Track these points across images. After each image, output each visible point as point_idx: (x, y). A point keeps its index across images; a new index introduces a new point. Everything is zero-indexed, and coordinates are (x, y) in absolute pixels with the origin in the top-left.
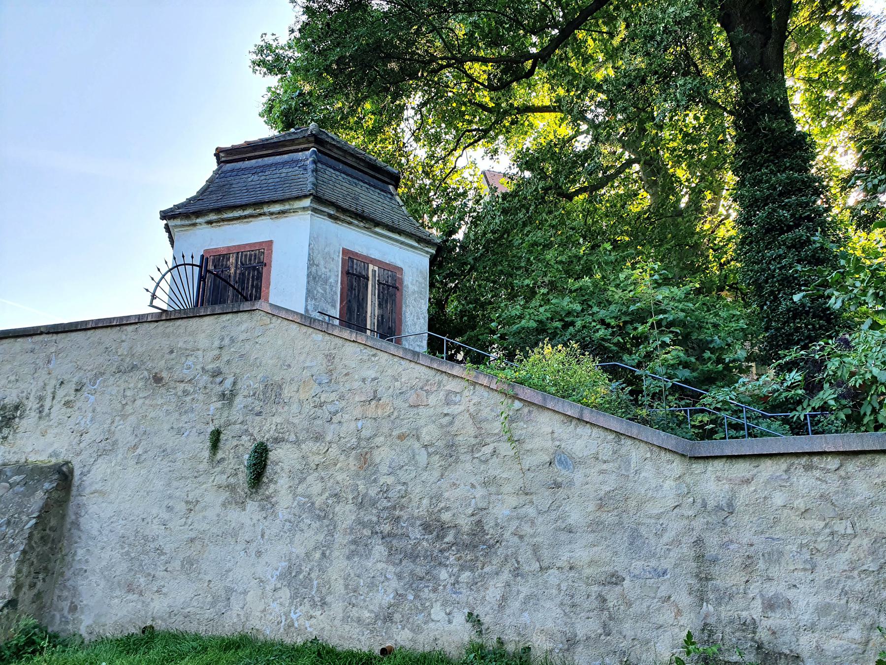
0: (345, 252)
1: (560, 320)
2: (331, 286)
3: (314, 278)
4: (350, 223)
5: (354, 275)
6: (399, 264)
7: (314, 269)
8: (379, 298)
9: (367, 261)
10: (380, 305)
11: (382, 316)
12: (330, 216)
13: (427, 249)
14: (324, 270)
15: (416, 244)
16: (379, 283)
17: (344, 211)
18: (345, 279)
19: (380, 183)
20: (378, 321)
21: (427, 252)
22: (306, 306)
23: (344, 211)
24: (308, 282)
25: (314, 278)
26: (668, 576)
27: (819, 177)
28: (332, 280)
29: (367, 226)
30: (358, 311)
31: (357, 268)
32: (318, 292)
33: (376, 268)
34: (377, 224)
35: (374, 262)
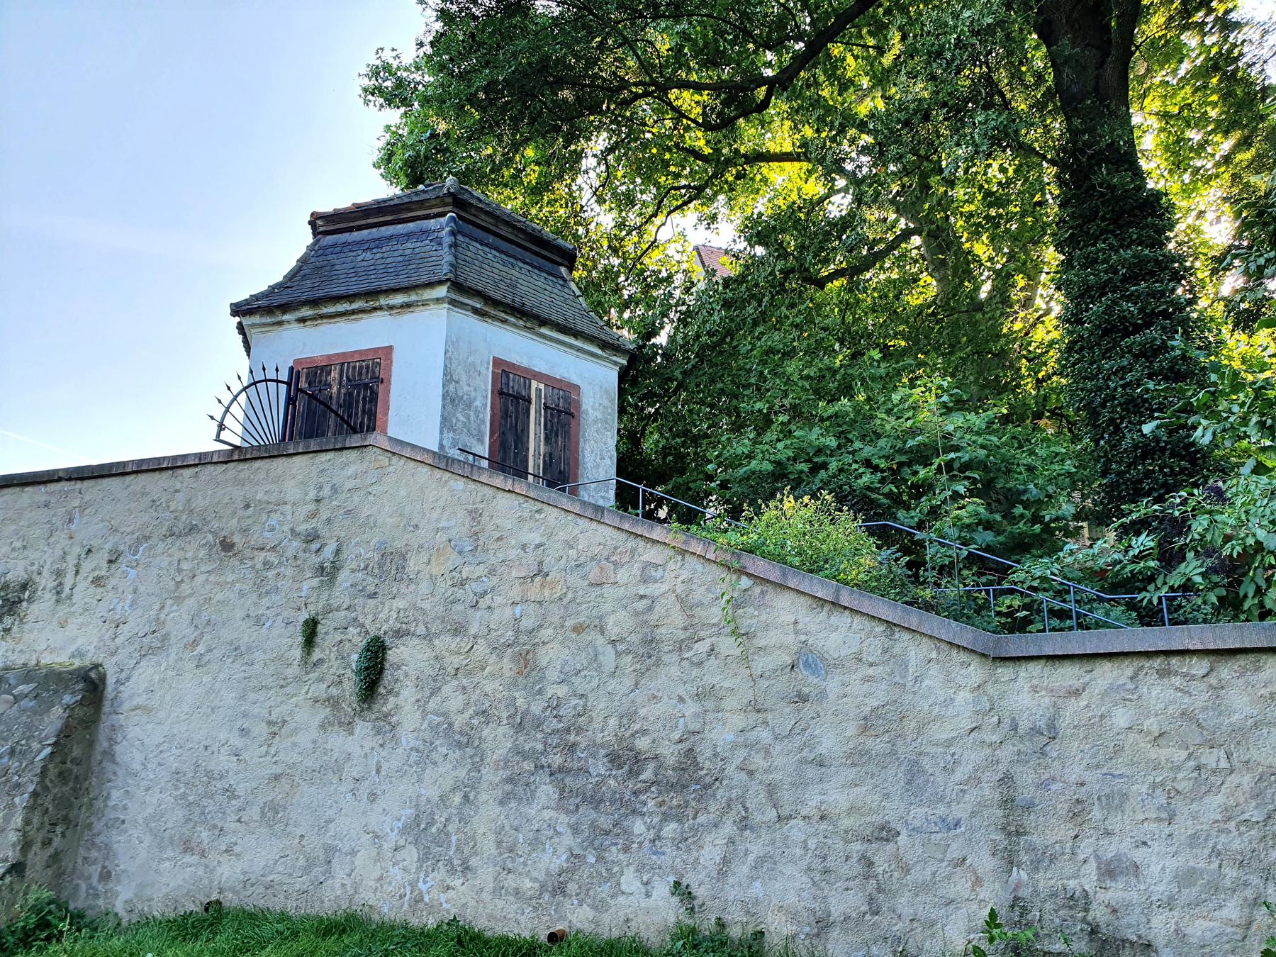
0: (497, 362)
2: (477, 412)
3: (453, 401)
4: (504, 321)
5: (510, 395)
6: (575, 380)
7: (452, 387)
8: (545, 428)
9: (529, 375)
10: (547, 438)
11: (551, 454)
12: (476, 311)
13: (614, 358)
14: (466, 388)
15: (599, 352)
16: (546, 408)
17: (496, 303)
18: (498, 401)
20: (544, 461)
21: (615, 363)
22: (441, 440)
23: (496, 303)
24: (444, 406)
25: (453, 401)
27: (1180, 255)
28: (477, 403)
29: (528, 325)
30: (516, 448)
31: (515, 386)
32: (458, 420)
33: (542, 386)
34: (544, 322)
35: (539, 376)
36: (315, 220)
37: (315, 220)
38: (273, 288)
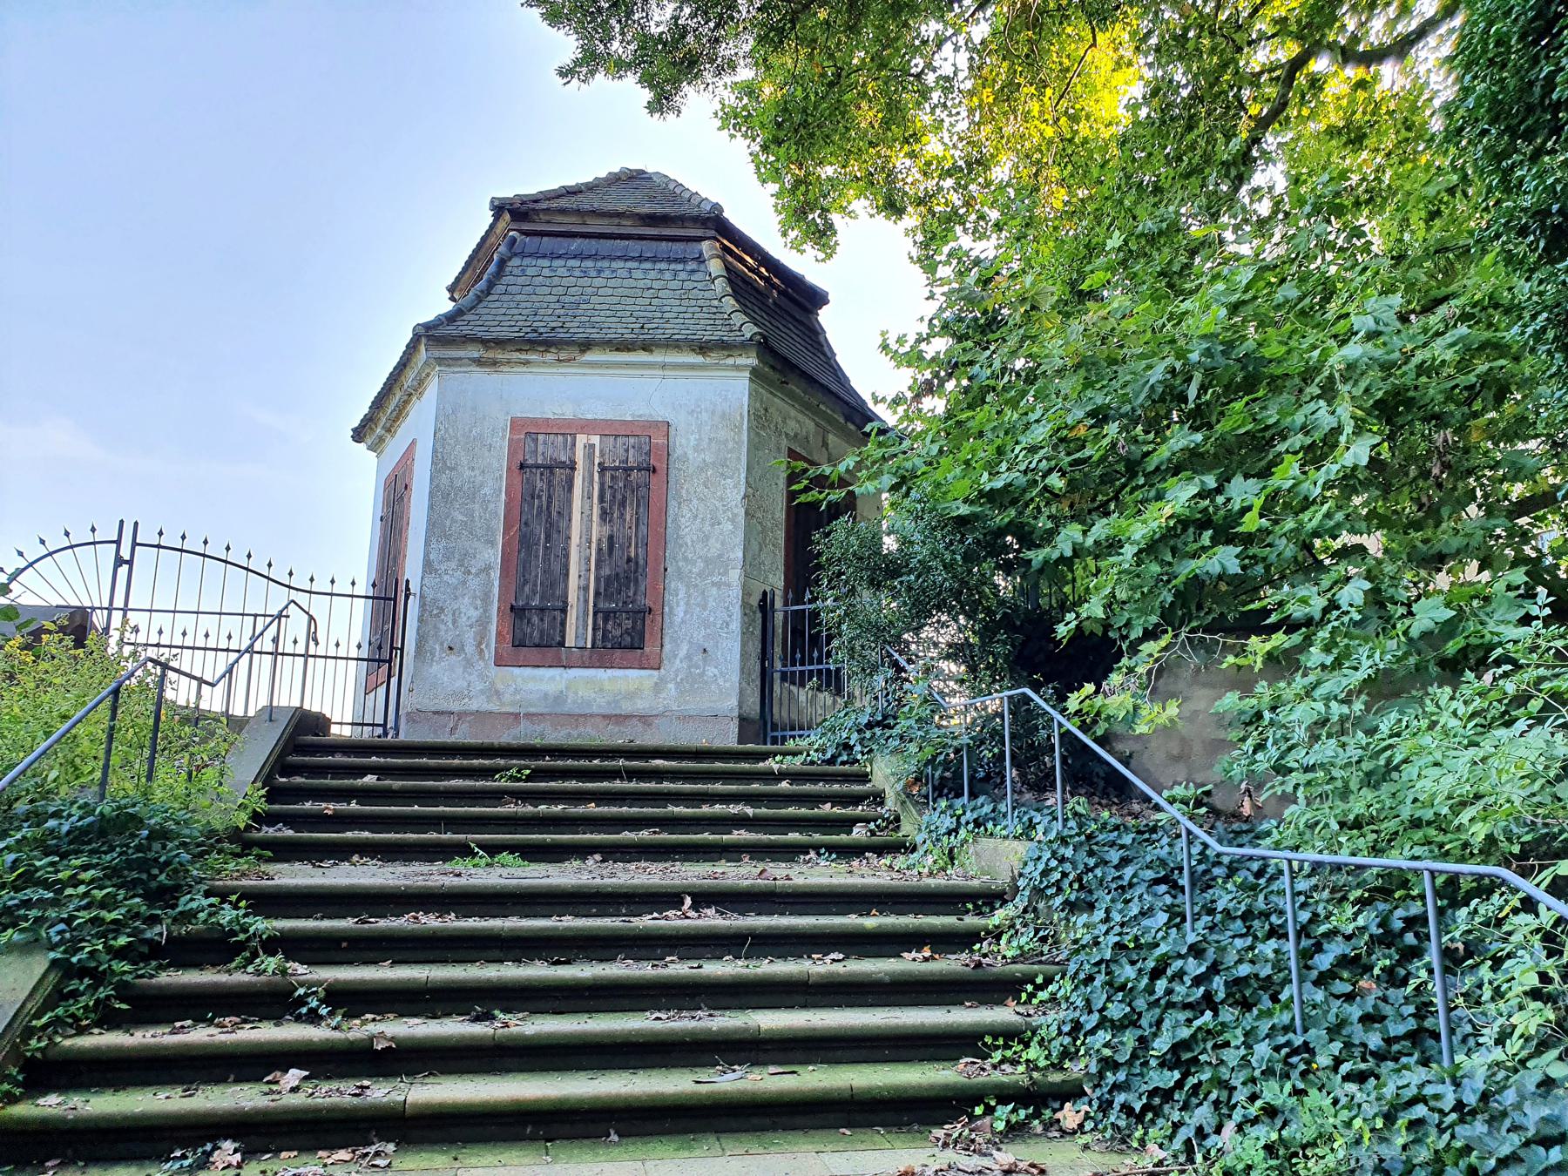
0: (516, 424)
1: (1515, 564)
2: (485, 502)
3: (446, 496)
4: (526, 363)
5: (538, 467)
6: (660, 413)
7: (444, 479)
8: (602, 499)
9: (568, 430)
10: (605, 515)
11: (611, 538)
12: (479, 362)
13: (730, 361)
14: (468, 473)
15: (699, 359)
16: (603, 469)
17: (500, 343)
18: (517, 480)
19: (564, 242)
20: (599, 550)
21: (737, 367)
22: (427, 554)
23: (500, 343)
24: (431, 507)
25: (446, 496)
26: (1202, 128)
27: (1544, 494)
28: (486, 490)
29: (563, 355)
30: (548, 538)
31: (549, 449)
32: (454, 521)
33: (596, 440)
34: (586, 346)
35: (588, 426)
36: (499, 208)
37: (499, 208)
38: (438, 318)
